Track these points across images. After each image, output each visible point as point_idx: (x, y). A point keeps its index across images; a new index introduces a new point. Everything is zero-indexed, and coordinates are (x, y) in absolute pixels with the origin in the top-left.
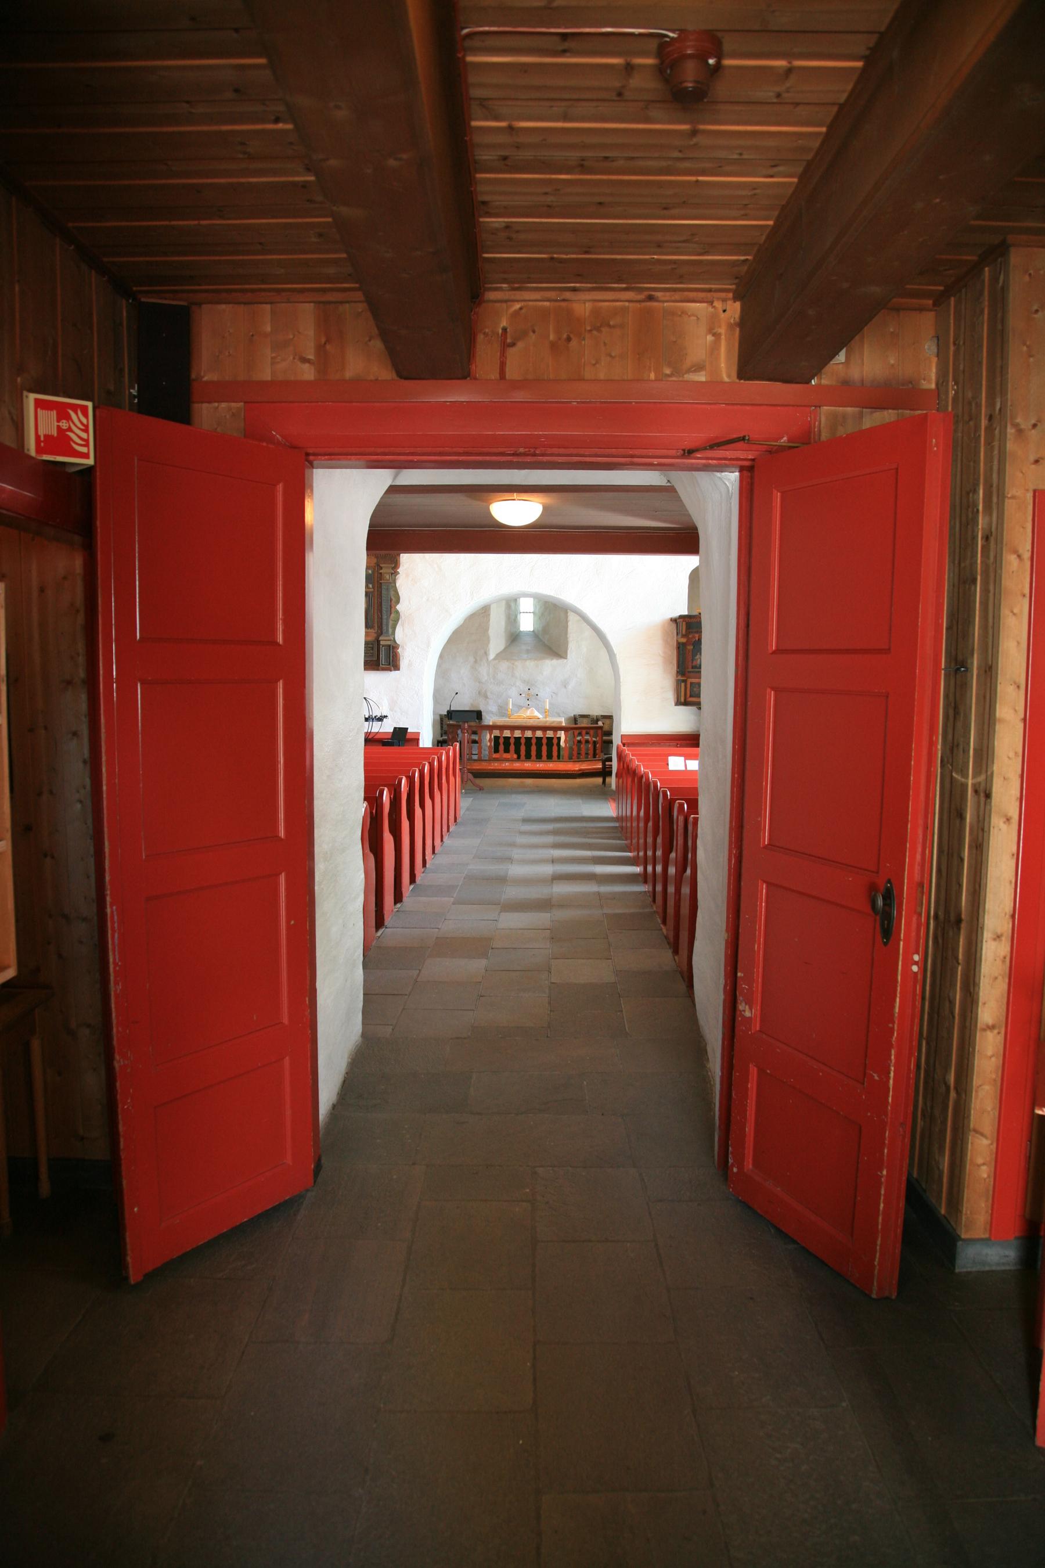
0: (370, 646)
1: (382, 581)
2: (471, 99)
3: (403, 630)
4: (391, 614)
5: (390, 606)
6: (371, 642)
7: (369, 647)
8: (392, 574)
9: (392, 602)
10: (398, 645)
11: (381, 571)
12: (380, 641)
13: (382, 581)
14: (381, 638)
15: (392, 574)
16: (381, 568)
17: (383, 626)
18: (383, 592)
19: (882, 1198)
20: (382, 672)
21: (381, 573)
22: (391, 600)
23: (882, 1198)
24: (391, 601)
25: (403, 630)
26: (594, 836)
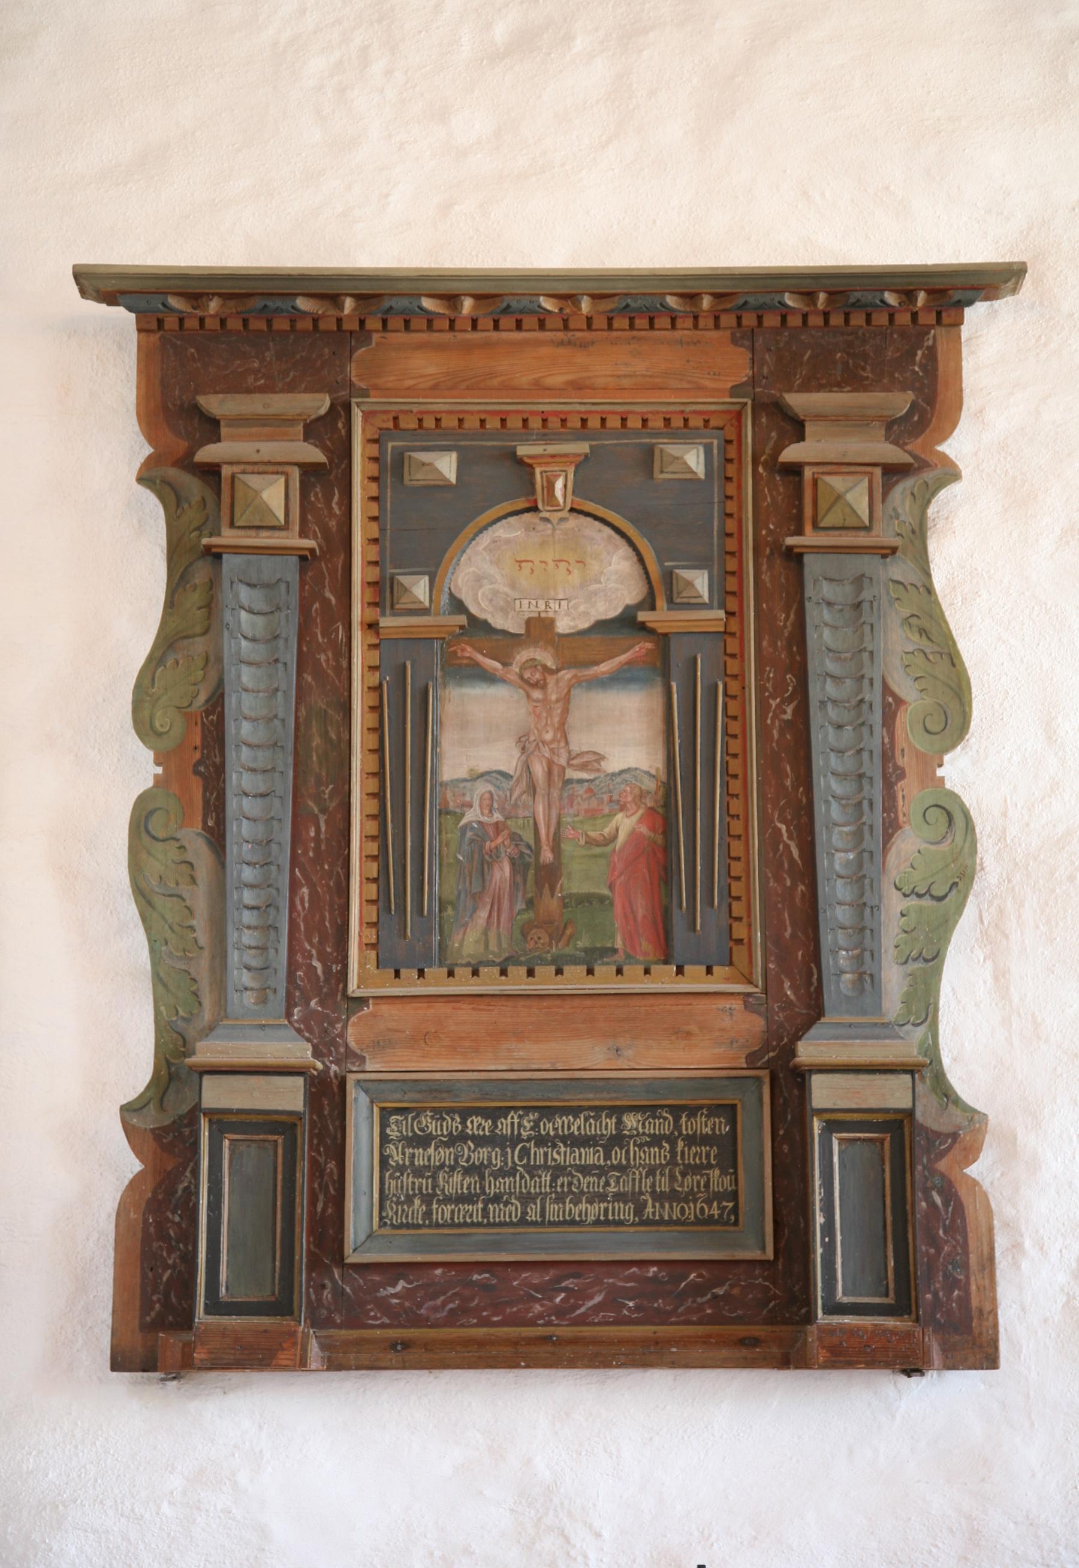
0: (703, 1125)
1: (809, 538)
2: (851, 905)
3: (1000, 976)
4: (891, 828)
5: (887, 756)
6: (704, 1084)
7: (691, 1140)
8: (893, 472)
9: (904, 720)
10: (972, 1114)
11: (792, 453)
12: (800, 1077)
13: (809, 538)
14: (807, 1051)
15: (893, 472)
16: (796, 428)
17: (827, 940)
18: (812, 636)
19: (788, 922)
20: (837, 1377)
21: (794, 470)
22: (892, 706)
23: (788, 922)
24: (889, 719)
25: (1000, 976)
26: (254, 430)
